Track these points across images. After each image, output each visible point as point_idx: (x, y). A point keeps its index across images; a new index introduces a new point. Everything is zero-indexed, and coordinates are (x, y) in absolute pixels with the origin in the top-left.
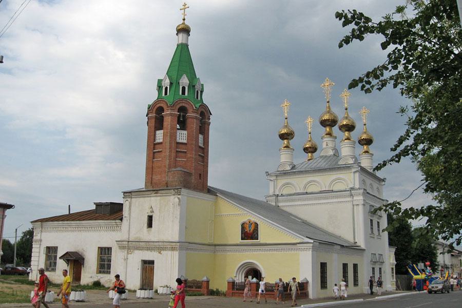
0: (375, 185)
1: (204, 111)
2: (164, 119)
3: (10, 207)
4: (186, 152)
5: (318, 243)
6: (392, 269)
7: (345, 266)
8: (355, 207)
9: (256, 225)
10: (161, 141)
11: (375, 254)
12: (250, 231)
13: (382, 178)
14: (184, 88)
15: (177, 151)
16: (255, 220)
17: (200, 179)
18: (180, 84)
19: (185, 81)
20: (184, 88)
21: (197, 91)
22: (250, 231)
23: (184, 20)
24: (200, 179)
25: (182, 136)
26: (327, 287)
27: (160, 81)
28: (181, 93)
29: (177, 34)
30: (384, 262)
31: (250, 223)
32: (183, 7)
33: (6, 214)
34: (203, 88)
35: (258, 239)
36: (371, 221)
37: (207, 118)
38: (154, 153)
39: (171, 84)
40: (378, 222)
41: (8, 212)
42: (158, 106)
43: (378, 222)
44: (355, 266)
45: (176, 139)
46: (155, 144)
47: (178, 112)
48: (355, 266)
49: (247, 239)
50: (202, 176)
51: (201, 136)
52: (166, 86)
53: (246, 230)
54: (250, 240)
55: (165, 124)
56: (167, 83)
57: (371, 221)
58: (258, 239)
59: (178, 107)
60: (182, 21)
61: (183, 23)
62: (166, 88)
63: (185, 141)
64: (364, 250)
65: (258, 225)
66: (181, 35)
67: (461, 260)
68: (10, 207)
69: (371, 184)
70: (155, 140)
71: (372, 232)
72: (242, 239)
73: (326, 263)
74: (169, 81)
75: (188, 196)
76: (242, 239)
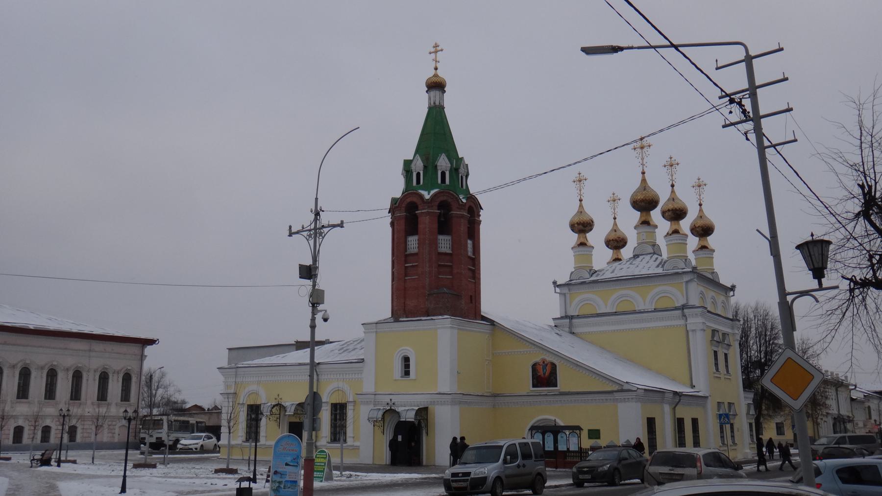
0: (720, 298)
1: (473, 206)
2: (419, 220)
3: (151, 342)
4: (451, 267)
5: (643, 391)
6: (751, 424)
7: (680, 422)
8: (679, 312)
9: (554, 366)
10: (416, 251)
11: (724, 403)
12: (544, 374)
13: (729, 285)
14: (443, 174)
15: (439, 266)
16: (550, 359)
17: (471, 302)
18: (439, 168)
19: (443, 163)
20: (443, 174)
21: (462, 177)
22: (544, 374)
23: (436, 69)
24: (471, 302)
25: (444, 243)
26: (685, 444)
27: (407, 164)
28: (439, 181)
29: (427, 92)
30: (737, 415)
31: (545, 364)
32: (433, 50)
33: (145, 354)
34: (468, 172)
35: (556, 386)
36: (715, 353)
37: (476, 215)
38: (406, 267)
39: (425, 167)
40: (726, 355)
41: (149, 350)
42: (409, 200)
43: (726, 355)
44: (695, 422)
45: (436, 248)
46: (406, 256)
47: (438, 210)
48: (695, 422)
49: (541, 387)
50: (473, 298)
51: (470, 242)
52: (418, 171)
53: (539, 374)
54: (546, 387)
55: (421, 226)
56: (418, 166)
57: (715, 353)
58: (556, 386)
59: (437, 203)
60: (433, 72)
61: (436, 76)
62: (418, 174)
63: (449, 251)
64: (706, 397)
65: (556, 366)
66: (432, 93)
67: (869, 407)
68: (151, 342)
69: (713, 298)
70: (406, 250)
71: (717, 370)
72: (534, 386)
73: (654, 418)
74: (422, 164)
75: (459, 329)
76: (534, 386)
